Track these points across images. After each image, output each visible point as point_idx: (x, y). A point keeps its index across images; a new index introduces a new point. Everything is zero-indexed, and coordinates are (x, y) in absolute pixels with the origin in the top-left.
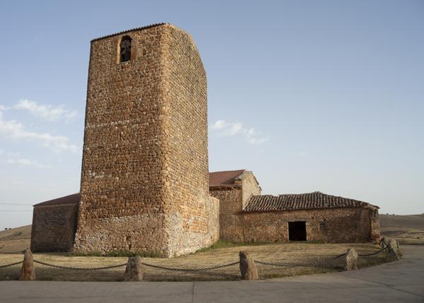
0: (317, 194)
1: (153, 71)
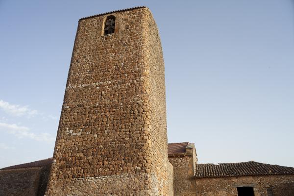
0: (253, 162)
1: (135, 41)
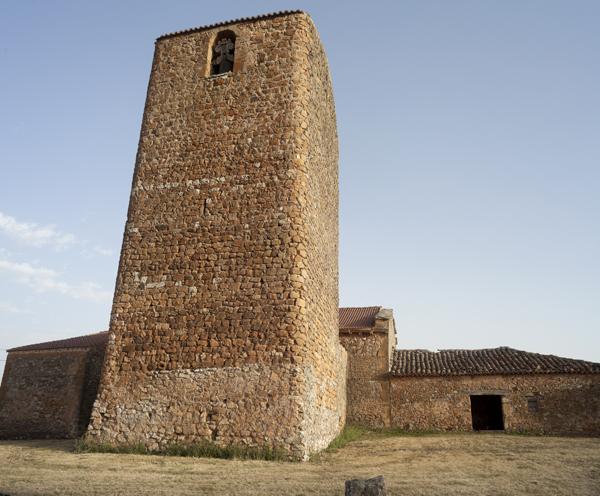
0: (507, 349)
1: (277, 91)
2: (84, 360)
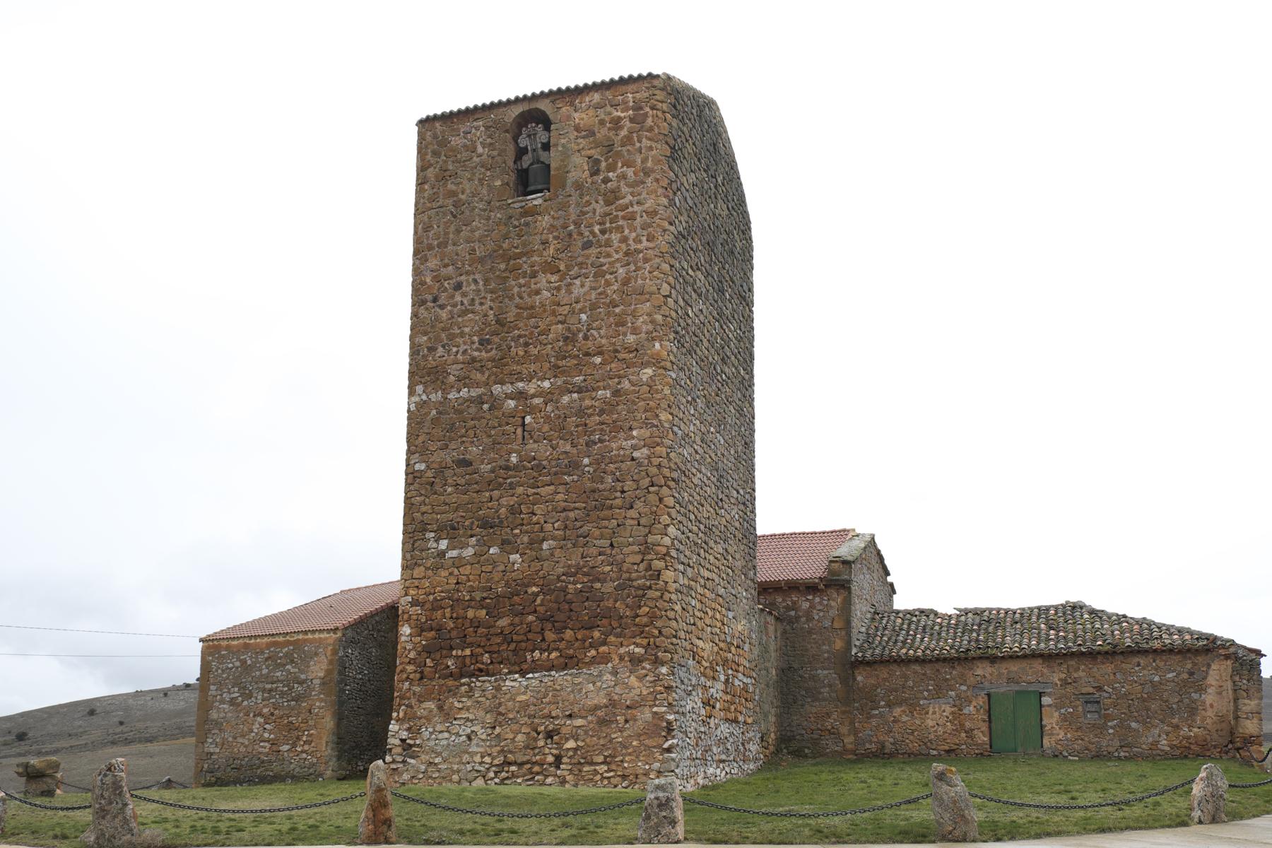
0: (1075, 608)
2: (335, 652)
